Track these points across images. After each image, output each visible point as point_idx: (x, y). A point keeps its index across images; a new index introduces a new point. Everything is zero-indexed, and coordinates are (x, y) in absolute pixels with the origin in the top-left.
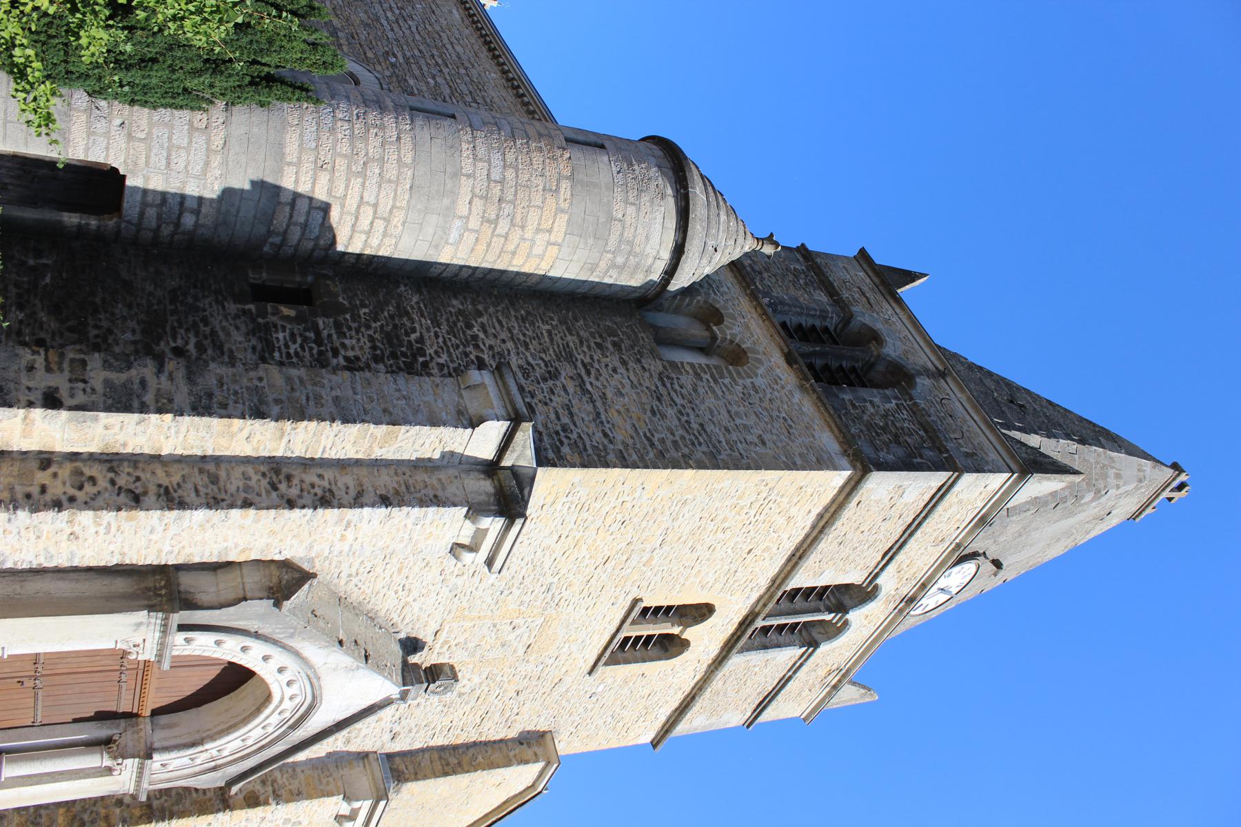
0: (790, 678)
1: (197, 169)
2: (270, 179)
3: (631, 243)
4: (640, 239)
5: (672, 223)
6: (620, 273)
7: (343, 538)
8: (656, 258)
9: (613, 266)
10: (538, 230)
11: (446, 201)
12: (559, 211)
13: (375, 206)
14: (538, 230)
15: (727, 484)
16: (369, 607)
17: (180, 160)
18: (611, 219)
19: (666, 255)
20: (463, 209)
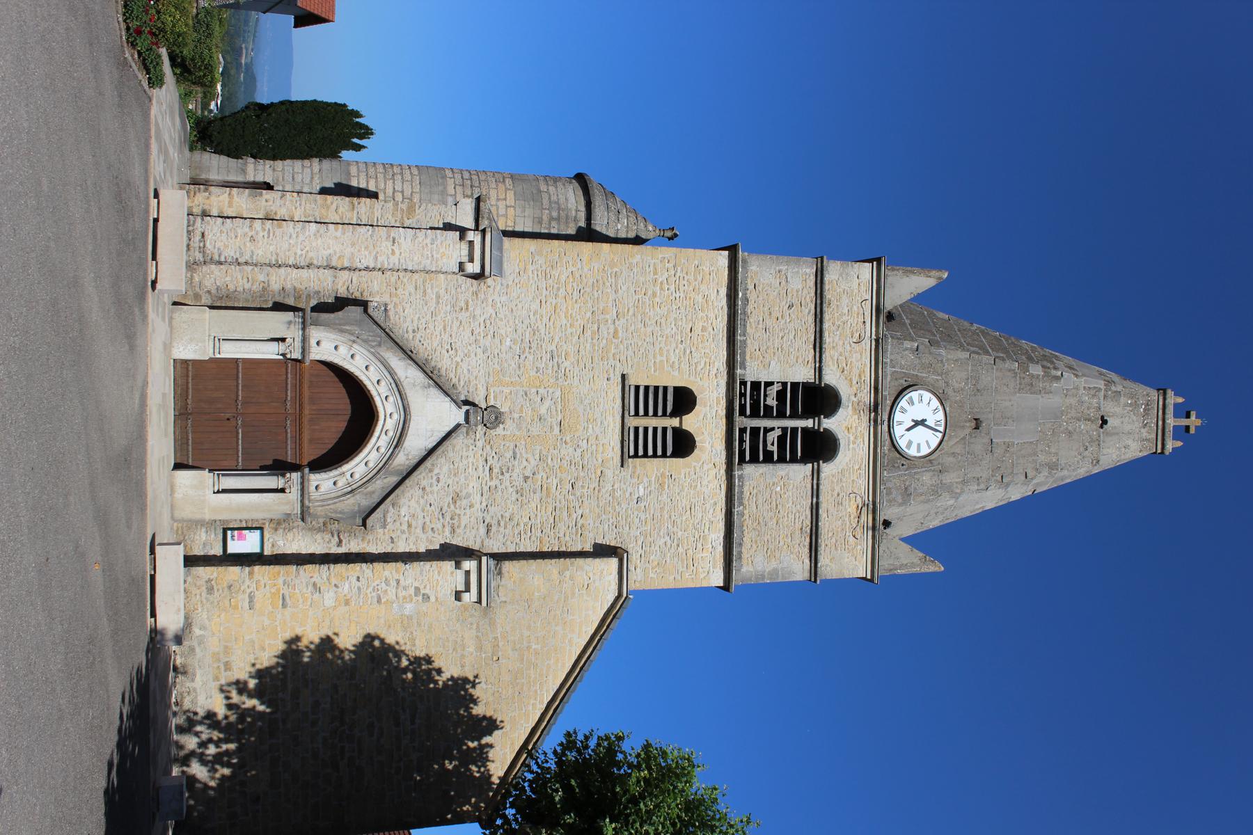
0: (817, 504)
1: (308, 181)
2: (344, 182)
3: (557, 203)
4: (562, 200)
5: (580, 193)
6: (559, 224)
7: (393, 252)
8: (577, 211)
9: (551, 219)
10: (498, 200)
11: (441, 188)
12: (507, 189)
13: (402, 192)
14: (498, 200)
15: (638, 258)
16: (433, 364)
17: (299, 178)
18: (540, 191)
19: (583, 208)
20: (451, 190)
